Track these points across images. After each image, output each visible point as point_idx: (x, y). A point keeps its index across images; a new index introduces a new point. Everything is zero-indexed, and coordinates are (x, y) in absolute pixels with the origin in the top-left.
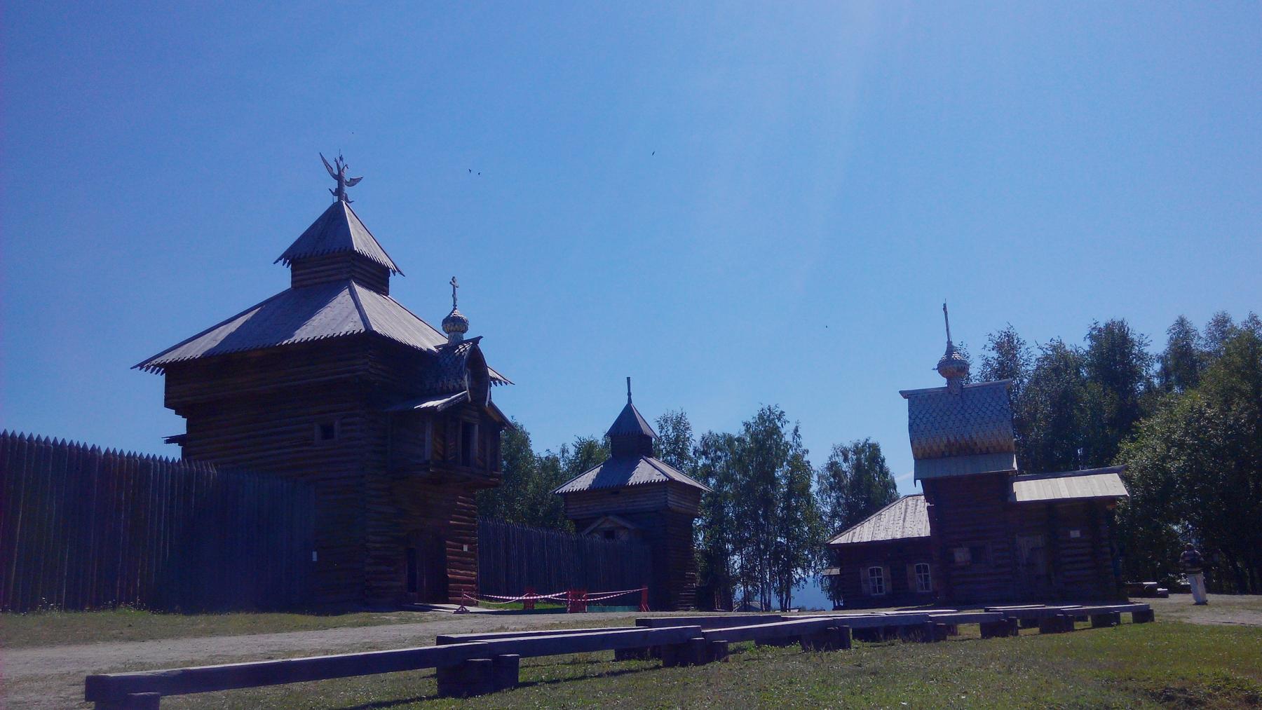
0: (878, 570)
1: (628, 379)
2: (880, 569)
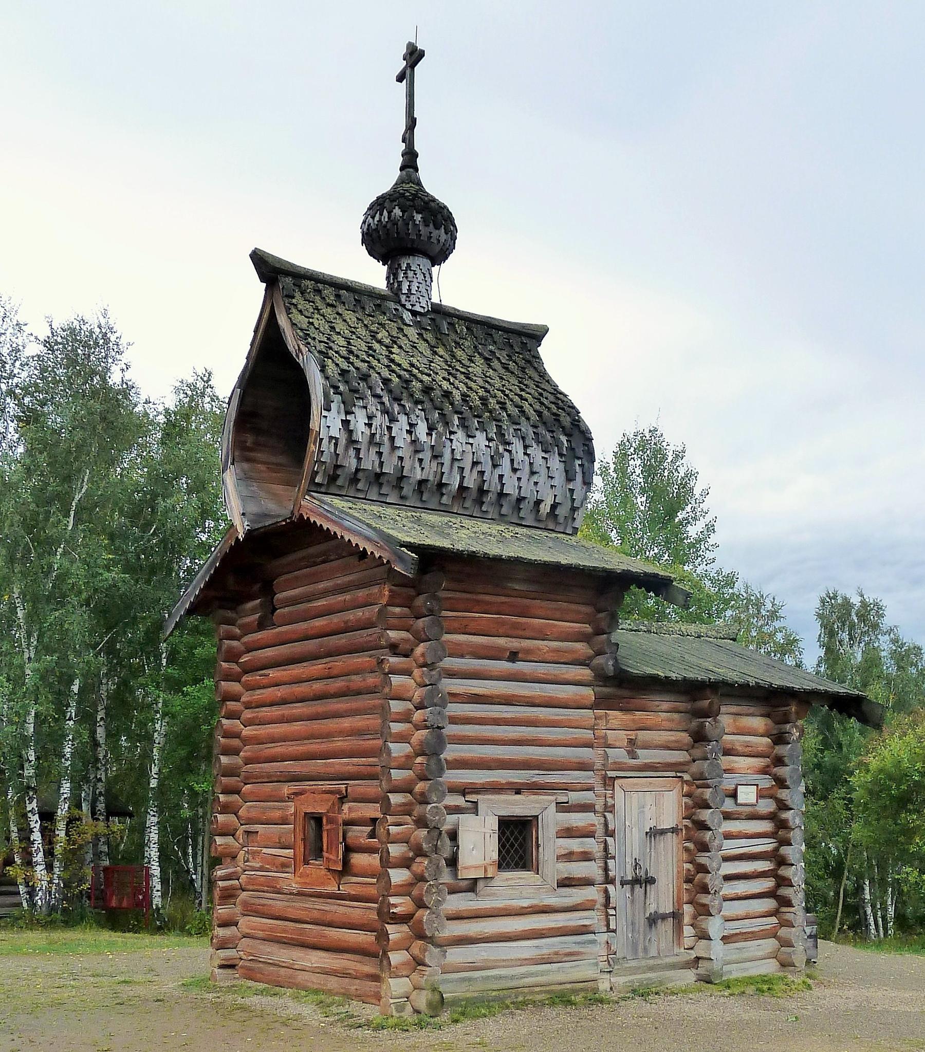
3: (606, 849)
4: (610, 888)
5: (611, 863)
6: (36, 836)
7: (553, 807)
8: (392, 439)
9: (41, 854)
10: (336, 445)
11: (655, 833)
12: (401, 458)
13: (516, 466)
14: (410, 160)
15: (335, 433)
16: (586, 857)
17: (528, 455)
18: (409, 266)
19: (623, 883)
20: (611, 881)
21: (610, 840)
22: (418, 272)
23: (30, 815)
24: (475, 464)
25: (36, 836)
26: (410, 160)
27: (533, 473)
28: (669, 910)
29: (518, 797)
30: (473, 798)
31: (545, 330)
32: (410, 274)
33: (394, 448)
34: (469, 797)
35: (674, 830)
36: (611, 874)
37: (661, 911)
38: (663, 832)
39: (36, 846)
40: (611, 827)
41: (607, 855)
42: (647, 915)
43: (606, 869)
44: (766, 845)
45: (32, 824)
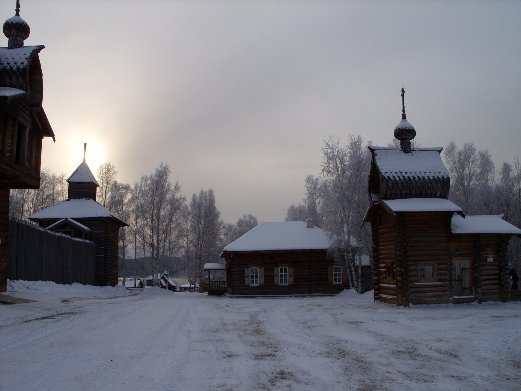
0: (286, 269)
1: (85, 144)
2: (258, 269)
3: (451, 273)
4: (452, 282)
5: (452, 276)
6: (353, 273)
7: (436, 264)
8: (398, 186)
9: (355, 278)
10: (385, 189)
11: (464, 269)
12: (400, 190)
13: (429, 187)
14: (404, 117)
15: (385, 187)
16: (445, 274)
17: (432, 184)
18: (404, 142)
19: (455, 280)
20: (452, 280)
21: (452, 271)
22: (407, 143)
23: (351, 267)
24: (418, 188)
25: (353, 273)
26: (404, 117)
27: (433, 188)
28: (468, 287)
29: (427, 262)
30: (416, 262)
31: (451, 141)
32: (405, 144)
33: (398, 188)
34: (415, 262)
35: (469, 268)
36: (452, 278)
37: (466, 287)
38: (466, 269)
39: (353, 275)
40: (452, 268)
41: (451, 274)
42: (462, 288)
43: (451, 277)
44: (496, 272)
45: (352, 270)
